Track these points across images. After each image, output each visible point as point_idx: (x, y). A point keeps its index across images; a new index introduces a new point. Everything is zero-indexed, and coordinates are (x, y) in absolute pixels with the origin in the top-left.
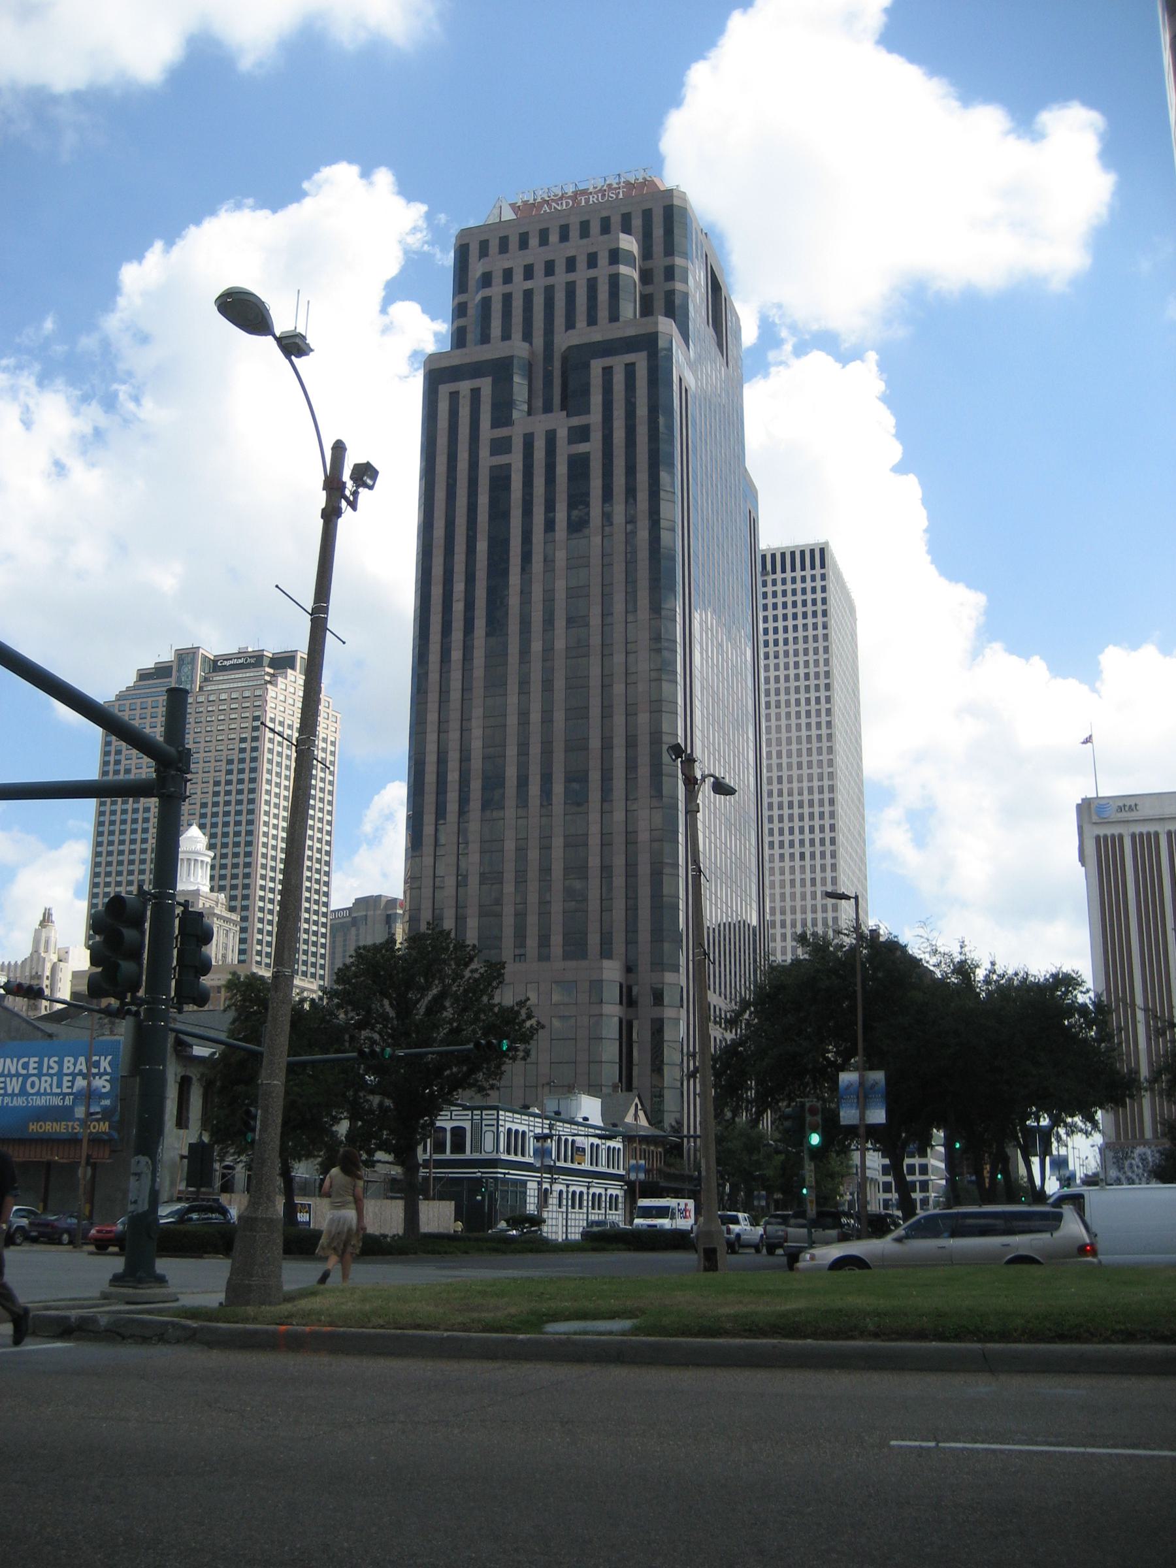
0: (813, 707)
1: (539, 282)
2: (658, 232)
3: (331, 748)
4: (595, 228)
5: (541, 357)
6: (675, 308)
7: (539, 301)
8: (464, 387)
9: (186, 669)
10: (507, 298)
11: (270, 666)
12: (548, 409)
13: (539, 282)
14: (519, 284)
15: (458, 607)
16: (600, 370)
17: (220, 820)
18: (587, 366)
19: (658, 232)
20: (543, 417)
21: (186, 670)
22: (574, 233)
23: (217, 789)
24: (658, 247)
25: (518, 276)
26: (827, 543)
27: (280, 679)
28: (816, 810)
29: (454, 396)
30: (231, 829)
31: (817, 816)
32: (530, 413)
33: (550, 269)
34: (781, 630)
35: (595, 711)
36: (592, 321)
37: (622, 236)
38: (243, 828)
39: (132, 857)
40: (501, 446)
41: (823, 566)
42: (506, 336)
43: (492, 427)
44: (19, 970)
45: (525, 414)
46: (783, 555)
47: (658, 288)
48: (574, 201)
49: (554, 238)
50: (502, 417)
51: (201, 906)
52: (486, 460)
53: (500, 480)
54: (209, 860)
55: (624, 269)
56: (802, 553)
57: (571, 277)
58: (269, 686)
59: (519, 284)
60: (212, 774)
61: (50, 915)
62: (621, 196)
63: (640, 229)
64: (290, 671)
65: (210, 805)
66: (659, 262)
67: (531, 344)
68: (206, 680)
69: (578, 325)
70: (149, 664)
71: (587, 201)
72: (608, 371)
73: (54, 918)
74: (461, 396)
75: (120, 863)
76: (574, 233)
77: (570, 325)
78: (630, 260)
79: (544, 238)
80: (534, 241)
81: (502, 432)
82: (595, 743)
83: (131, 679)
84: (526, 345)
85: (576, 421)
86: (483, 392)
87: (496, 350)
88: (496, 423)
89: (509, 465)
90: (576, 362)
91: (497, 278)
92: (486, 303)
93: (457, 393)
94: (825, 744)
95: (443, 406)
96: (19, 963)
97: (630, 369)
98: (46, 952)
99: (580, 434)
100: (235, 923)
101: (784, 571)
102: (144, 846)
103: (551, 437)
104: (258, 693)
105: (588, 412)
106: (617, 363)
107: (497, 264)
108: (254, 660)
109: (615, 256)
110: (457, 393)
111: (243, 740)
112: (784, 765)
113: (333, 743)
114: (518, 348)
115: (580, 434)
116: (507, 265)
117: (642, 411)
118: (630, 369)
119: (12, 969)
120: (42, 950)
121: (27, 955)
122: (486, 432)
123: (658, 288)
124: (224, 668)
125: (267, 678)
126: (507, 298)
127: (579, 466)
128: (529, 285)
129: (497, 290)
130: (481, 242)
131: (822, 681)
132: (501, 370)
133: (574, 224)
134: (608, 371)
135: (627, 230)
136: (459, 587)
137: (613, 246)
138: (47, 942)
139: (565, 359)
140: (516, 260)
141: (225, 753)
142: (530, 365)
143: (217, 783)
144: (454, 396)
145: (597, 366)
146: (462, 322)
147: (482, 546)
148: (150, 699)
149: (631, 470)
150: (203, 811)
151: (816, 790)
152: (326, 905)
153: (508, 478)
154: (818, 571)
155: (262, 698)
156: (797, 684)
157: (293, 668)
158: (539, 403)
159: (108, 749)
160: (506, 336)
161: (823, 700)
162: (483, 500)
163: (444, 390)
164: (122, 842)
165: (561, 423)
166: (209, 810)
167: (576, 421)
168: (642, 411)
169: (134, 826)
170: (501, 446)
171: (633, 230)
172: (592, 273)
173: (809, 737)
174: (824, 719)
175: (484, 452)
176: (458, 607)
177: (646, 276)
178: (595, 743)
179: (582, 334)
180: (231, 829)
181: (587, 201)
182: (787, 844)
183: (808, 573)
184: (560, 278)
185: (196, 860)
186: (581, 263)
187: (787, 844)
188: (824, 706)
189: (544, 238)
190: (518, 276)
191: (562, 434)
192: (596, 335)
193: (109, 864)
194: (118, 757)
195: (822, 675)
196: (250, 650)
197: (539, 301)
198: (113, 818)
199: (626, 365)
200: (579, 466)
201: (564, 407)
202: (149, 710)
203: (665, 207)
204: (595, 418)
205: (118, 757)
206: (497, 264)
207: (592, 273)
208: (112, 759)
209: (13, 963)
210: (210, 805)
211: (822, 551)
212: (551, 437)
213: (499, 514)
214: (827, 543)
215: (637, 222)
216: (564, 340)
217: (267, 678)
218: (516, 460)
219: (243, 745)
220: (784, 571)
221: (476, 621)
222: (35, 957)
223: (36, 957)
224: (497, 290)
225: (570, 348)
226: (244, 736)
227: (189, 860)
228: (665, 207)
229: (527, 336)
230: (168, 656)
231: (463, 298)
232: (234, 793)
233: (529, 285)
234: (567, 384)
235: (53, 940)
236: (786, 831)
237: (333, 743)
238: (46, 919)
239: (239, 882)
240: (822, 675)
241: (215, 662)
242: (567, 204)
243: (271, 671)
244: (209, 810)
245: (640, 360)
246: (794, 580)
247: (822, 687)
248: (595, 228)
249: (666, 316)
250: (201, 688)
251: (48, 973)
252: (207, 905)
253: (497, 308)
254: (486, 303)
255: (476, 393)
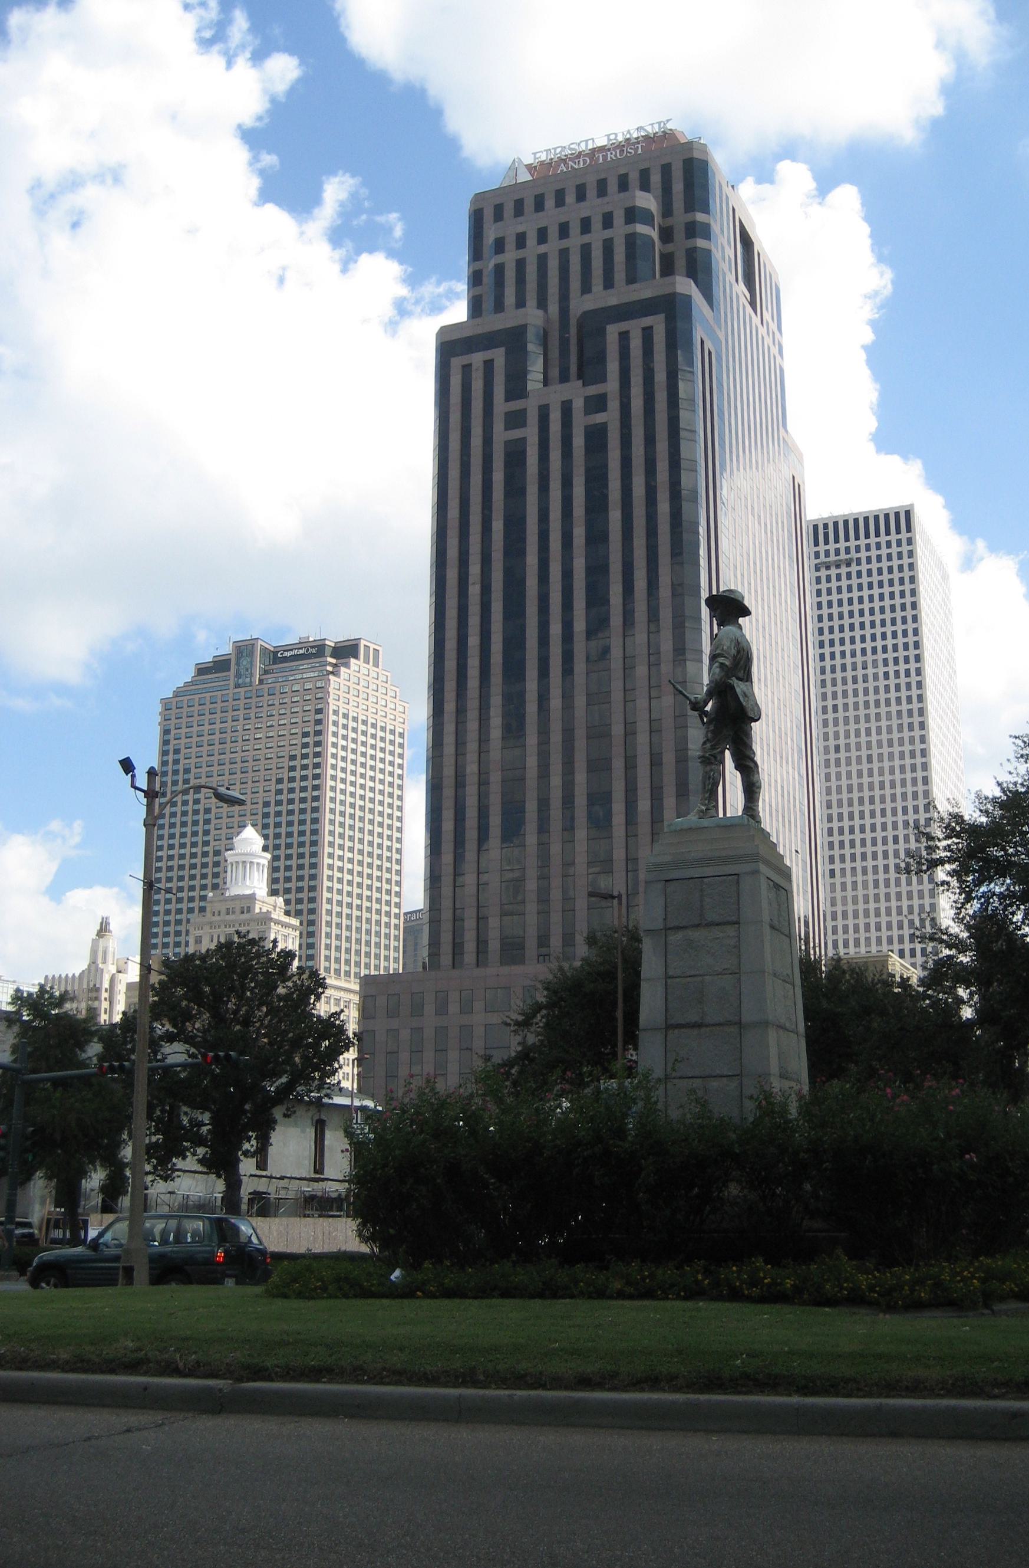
0: (903, 680)
1: (552, 247)
2: (678, 187)
3: (398, 740)
4: (613, 186)
5: (557, 325)
6: (699, 268)
7: (553, 265)
8: (477, 359)
9: (244, 662)
10: (521, 264)
11: (332, 656)
12: (564, 378)
13: (552, 247)
14: (533, 249)
15: (474, 590)
16: (616, 336)
17: (295, 818)
18: (602, 332)
19: (678, 187)
20: (559, 387)
21: (245, 663)
22: (591, 192)
23: (280, 787)
24: (678, 204)
25: (531, 240)
26: (912, 505)
27: (343, 669)
28: (899, 791)
29: (467, 369)
30: (295, 829)
31: (910, 796)
32: (546, 382)
33: (564, 231)
34: (866, 599)
35: (617, 695)
36: (609, 284)
37: (639, 194)
38: (307, 828)
39: (301, 861)
40: (515, 419)
41: (909, 529)
42: (521, 303)
43: (507, 400)
44: (77, 982)
45: (541, 385)
46: (856, 521)
47: (679, 246)
48: (591, 159)
49: (570, 198)
50: (516, 388)
51: (257, 911)
52: (501, 435)
53: (515, 456)
54: (266, 862)
55: (641, 229)
56: (856, 521)
57: (586, 238)
58: (331, 677)
59: (533, 249)
60: (275, 771)
61: (107, 924)
62: (640, 151)
63: (659, 185)
64: (353, 660)
65: (273, 804)
66: (680, 218)
67: (546, 311)
68: (266, 672)
69: (594, 289)
70: (207, 658)
71: (605, 157)
72: (624, 336)
73: (112, 927)
74: (474, 368)
75: (181, 867)
76: (591, 192)
77: (586, 289)
78: (647, 217)
79: (560, 199)
80: (550, 203)
81: (516, 405)
82: (617, 730)
83: (189, 675)
84: (540, 313)
85: (593, 390)
86: (496, 364)
87: (509, 319)
88: (510, 397)
89: (524, 439)
90: (593, 326)
91: (510, 244)
92: (499, 269)
93: (470, 365)
94: (916, 720)
95: (456, 381)
96: (77, 975)
97: (648, 332)
98: (104, 962)
99: (597, 404)
100: (294, 928)
101: (888, 533)
102: (206, 849)
103: (567, 409)
104: (319, 684)
105: (602, 378)
106: (635, 327)
107: (511, 228)
108: (317, 650)
109: (632, 215)
110: (470, 365)
111: (306, 735)
112: (874, 743)
113: (401, 735)
114: (533, 316)
115: (597, 404)
116: (520, 229)
117: (660, 377)
118: (648, 332)
119: (70, 981)
120: (100, 961)
121: (85, 967)
122: (501, 406)
123: (679, 246)
124: (285, 659)
125: (329, 668)
126: (521, 264)
127: (596, 437)
128: (543, 249)
129: (510, 257)
130: (663, 166)
131: (912, 652)
132: (514, 340)
133: (591, 181)
134: (624, 336)
135: (645, 187)
136: (475, 570)
137: (629, 204)
138: (105, 953)
139: (580, 326)
140: (529, 225)
141: (287, 748)
142: (546, 333)
143: (280, 781)
144: (467, 369)
145: (612, 331)
146: (478, 290)
147: (498, 526)
148: (197, 697)
149: (650, 440)
150: (266, 810)
151: (908, 768)
152: (398, 905)
153: (524, 452)
154: (904, 535)
155: (324, 689)
156: (885, 656)
157: (356, 657)
158: (555, 372)
159: (166, 748)
160: (521, 303)
161: (913, 673)
162: (498, 477)
163: (457, 363)
164: (194, 845)
165: (576, 392)
166: (272, 810)
167: (593, 390)
168: (660, 377)
169: (278, 830)
170: (515, 419)
171: (652, 186)
172: (608, 234)
173: (899, 713)
174: (914, 692)
175: (498, 426)
176: (474, 590)
177: (666, 235)
178: (617, 730)
179: (599, 298)
180: (295, 829)
181: (605, 157)
182: (879, 827)
183: (893, 537)
184: (575, 241)
185: (251, 863)
186: (597, 224)
187: (879, 827)
188: (914, 679)
189: (560, 199)
190: (531, 240)
191: (578, 404)
192: (612, 299)
193: (288, 868)
194: (176, 757)
195: (911, 646)
196: (311, 639)
197: (553, 265)
198: (173, 820)
199: (644, 329)
200: (596, 437)
201: (580, 376)
202: (219, 705)
203: (685, 161)
204: (612, 386)
205: (176, 757)
206: (511, 228)
207: (608, 234)
208: (170, 758)
209: (57, 976)
210: (273, 804)
211: (908, 513)
212: (567, 409)
213: (515, 490)
214: (912, 505)
215: (656, 178)
216: (581, 304)
217: (329, 668)
218: (531, 433)
219: (305, 740)
220: (888, 533)
221: (470, 608)
222: (93, 968)
223: (94, 969)
224: (510, 257)
225: (585, 313)
226: (305, 730)
227: (244, 862)
228: (685, 161)
229: (542, 304)
230: (227, 649)
231: (478, 265)
232: (285, 792)
233: (543, 249)
234: (582, 351)
235: (111, 950)
236: (878, 813)
237: (401, 735)
238: (104, 929)
239: (304, 884)
240: (911, 646)
241: (275, 653)
242: (585, 162)
243: (334, 661)
244: (272, 810)
245: (658, 323)
246: (889, 544)
247: (912, 659)
248: (613, 186)
249: (688, 276)
250: (261, 681)
251: (106, 984)
252: (264, 910)
253: (510, 275)
254: (499, 269)
255: (489, 364)
